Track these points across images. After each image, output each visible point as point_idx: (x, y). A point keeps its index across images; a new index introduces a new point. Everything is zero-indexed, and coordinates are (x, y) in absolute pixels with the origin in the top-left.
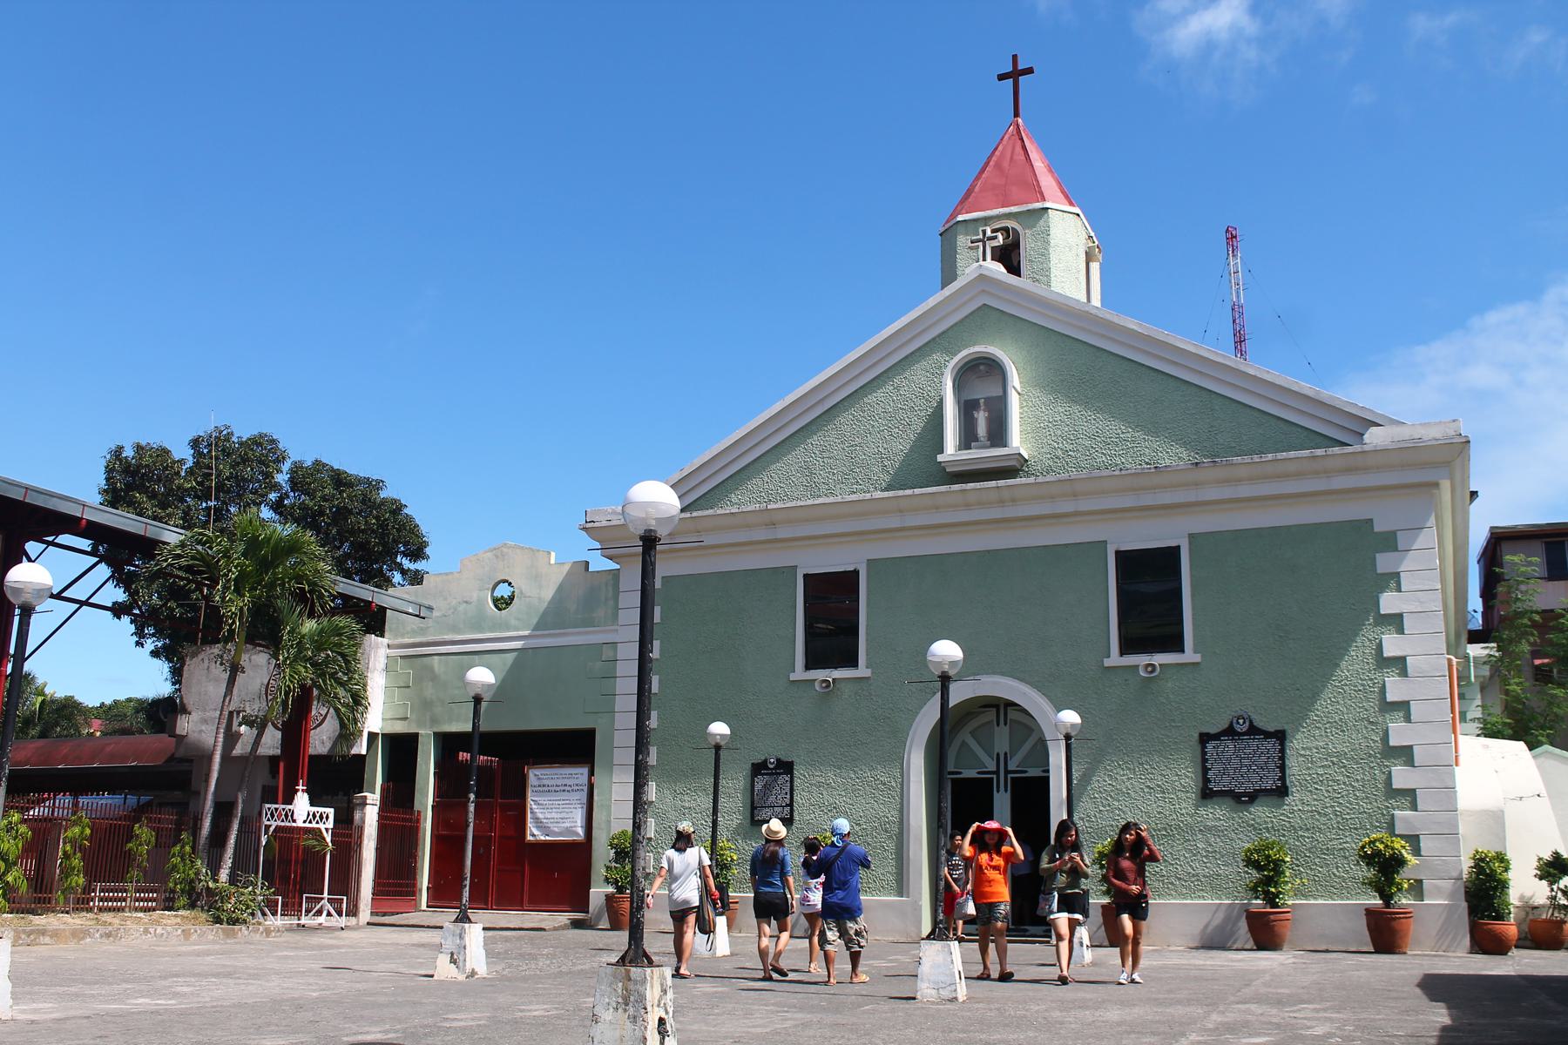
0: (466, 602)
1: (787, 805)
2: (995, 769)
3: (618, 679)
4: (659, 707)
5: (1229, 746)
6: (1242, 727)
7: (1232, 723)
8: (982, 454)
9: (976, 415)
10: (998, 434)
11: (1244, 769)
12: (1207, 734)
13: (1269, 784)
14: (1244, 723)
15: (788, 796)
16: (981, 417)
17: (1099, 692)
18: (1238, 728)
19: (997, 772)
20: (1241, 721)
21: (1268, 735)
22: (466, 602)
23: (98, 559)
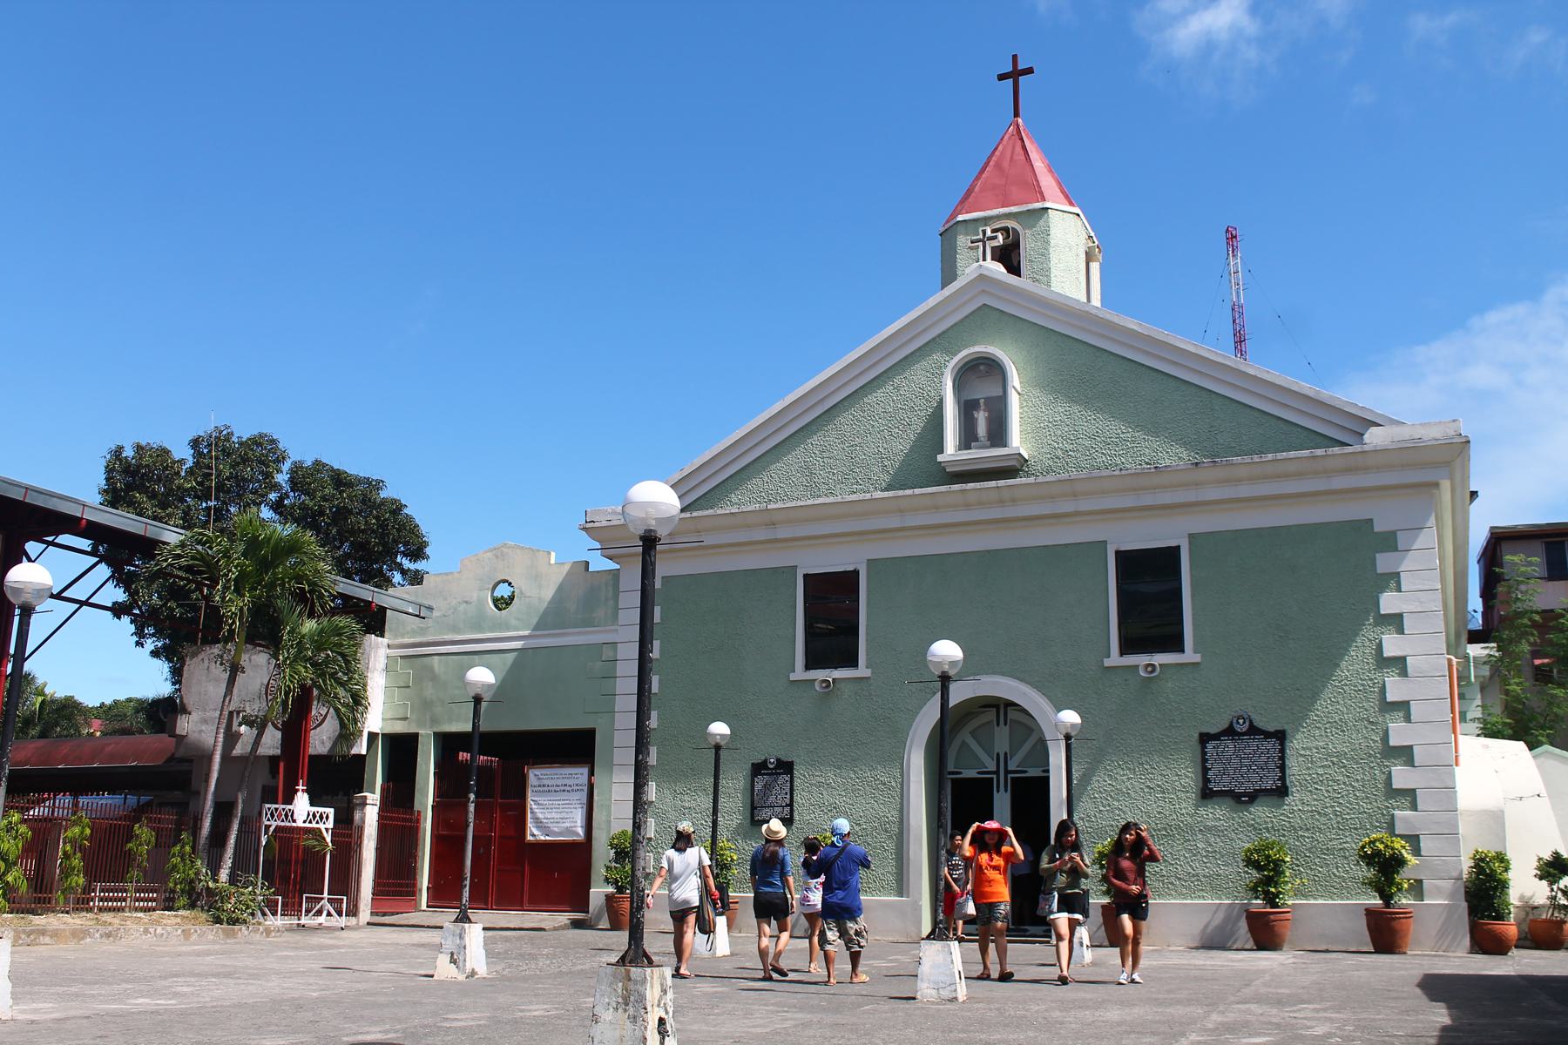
0: (466, 602)
1: (787, 805)
2: (995, 769)
3: (618, 679)
4: (659, 707)
5: (1229, 746)
6: (1242, 727)
7: (1232, 723)
8: (982, 454)
10: (998, 434)
11: (1245, 769)
12: (1207, 734)
13: (1269, 784)
14: (1244, 723)
15: (788, 796)
16: (981, 417)
17: (1099, 692)
18: (1238, 728)
19: (997, 773)
20: (1241, 721)
21: (1268, 735)
22: (466, 602)
23: (98, 559)
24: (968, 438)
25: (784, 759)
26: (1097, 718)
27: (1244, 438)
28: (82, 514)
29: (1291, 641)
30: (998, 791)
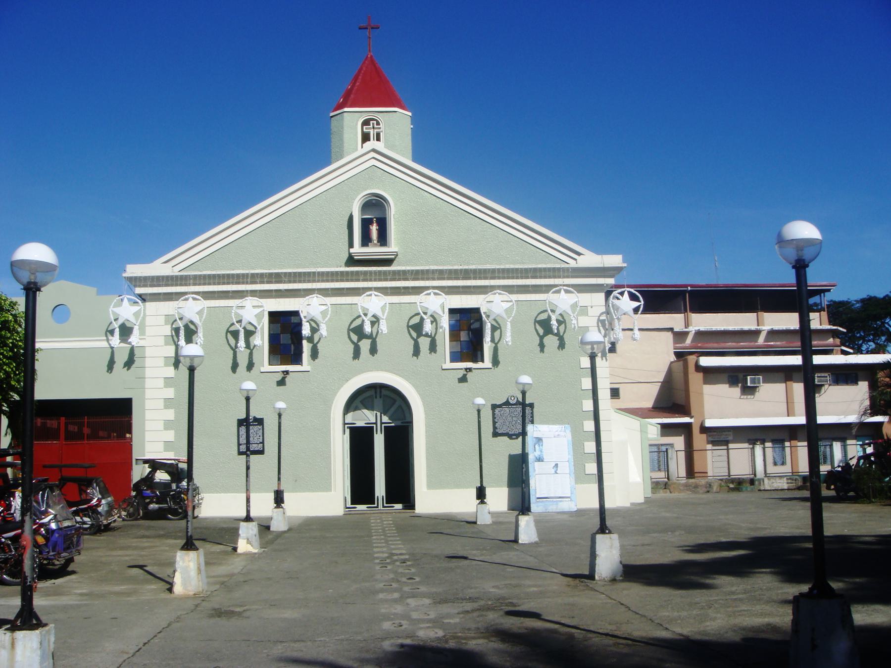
0: (217, 652)
1: (260, 443)
2: (375, 422)
3: (610, 503)
4: (176, 386)
5: (506, 410)
7: (508, 399)
8: (374, 250)
9: (371, 228)
10: (383, 239)
11: (514, 422)
14: (514, 399)
15: (261, 438)
16: (374, 228)
17: (439, 381)
18: (511, 402)
19: (376, 423)
20: (513, 398)
22: (217, 652)
23: (521, 437)
24: (366, 240)
25: (258, 417)
26: (438, 396)
27: (514, 253)
28: (247, 462)
29: (537, 359)
30: (377, 433)
